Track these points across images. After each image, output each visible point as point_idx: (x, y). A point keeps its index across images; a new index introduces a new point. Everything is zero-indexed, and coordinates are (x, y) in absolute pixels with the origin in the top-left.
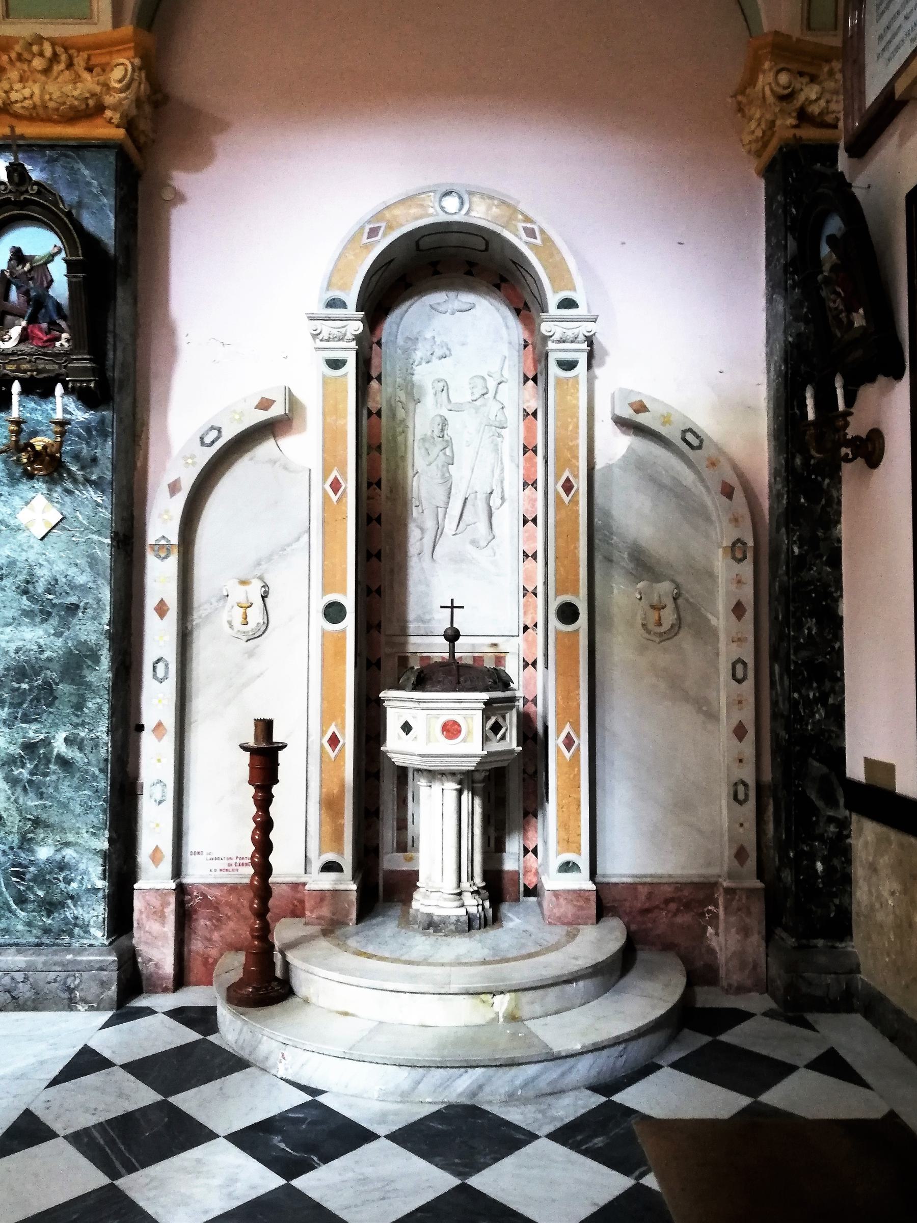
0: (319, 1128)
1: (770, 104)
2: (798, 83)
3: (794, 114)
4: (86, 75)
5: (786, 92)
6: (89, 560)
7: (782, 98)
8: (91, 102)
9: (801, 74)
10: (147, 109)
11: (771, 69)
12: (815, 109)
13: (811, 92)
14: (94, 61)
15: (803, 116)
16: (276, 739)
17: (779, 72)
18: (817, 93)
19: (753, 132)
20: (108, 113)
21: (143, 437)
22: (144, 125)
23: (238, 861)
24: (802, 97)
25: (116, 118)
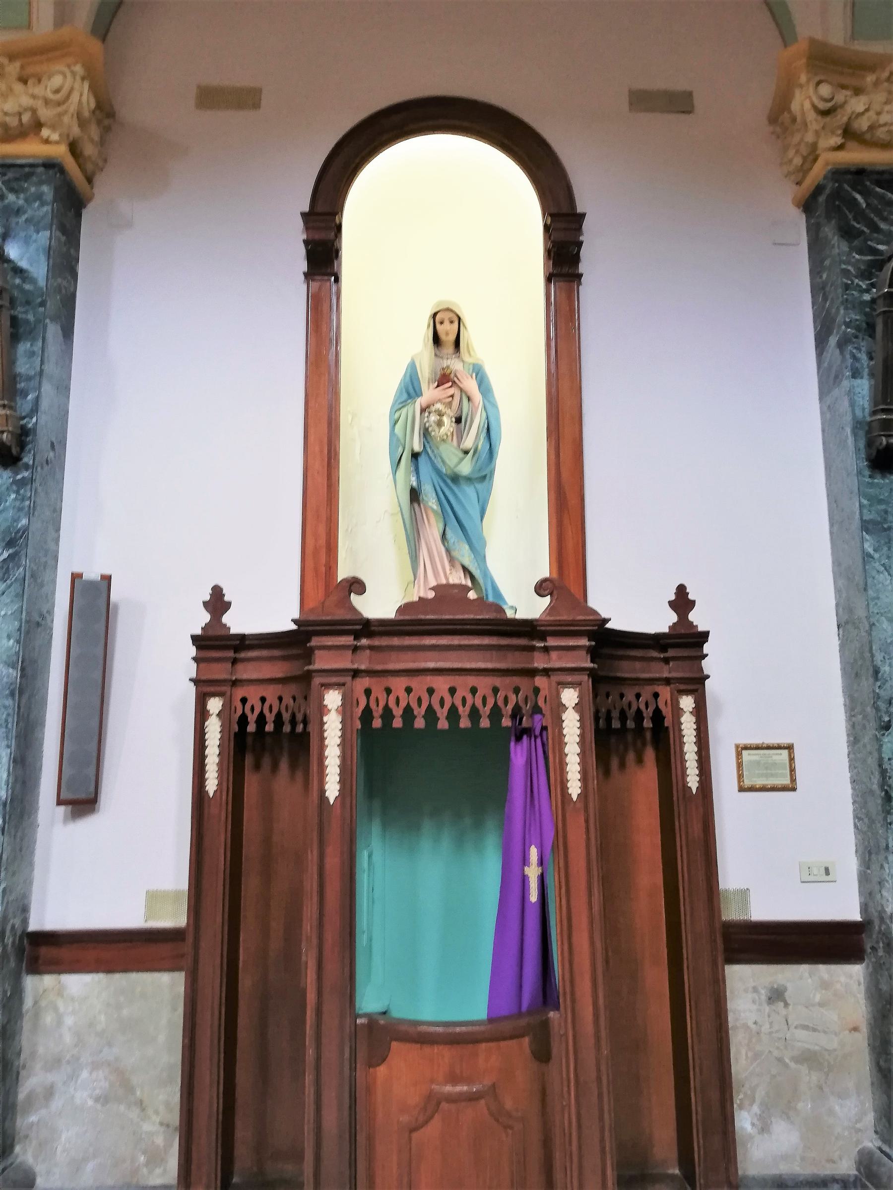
0: (848, 414)
1: (810, 121)
2: (840, 97)
3: (840, 132)
4: (18, 87)
5: (829, 105)
6: (34, 408)
7: (825, 113)
8: (26, 118)
9: (843, 87)
10: (94, 131)
11: (808, 81)
12: (863, 124)
13: (858, 104)
14: (30, 70)
15: (849, 133)
16: (343, 572)
17: (818, 83)
18: (864, 104)
19: (791, 161)
20: (45, 132)
21: (17, 1038)
22: (89, 150)
23: (299, 717)
24: (849, 109)
25: (55, 137)
